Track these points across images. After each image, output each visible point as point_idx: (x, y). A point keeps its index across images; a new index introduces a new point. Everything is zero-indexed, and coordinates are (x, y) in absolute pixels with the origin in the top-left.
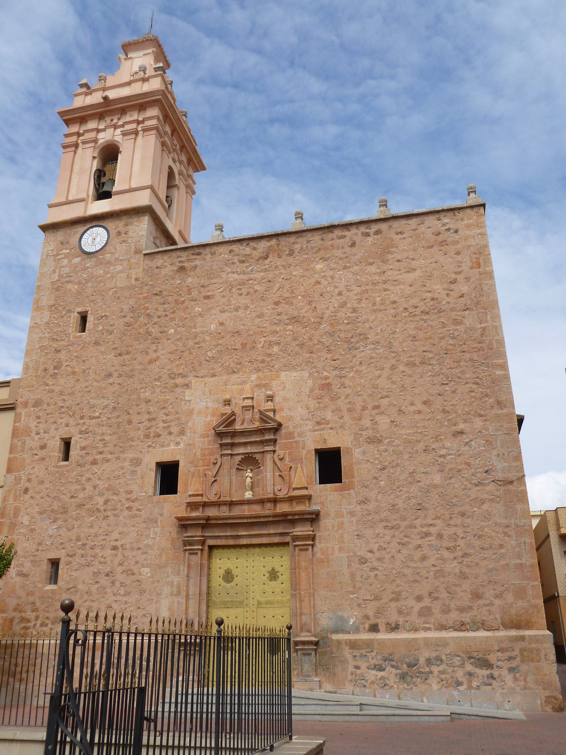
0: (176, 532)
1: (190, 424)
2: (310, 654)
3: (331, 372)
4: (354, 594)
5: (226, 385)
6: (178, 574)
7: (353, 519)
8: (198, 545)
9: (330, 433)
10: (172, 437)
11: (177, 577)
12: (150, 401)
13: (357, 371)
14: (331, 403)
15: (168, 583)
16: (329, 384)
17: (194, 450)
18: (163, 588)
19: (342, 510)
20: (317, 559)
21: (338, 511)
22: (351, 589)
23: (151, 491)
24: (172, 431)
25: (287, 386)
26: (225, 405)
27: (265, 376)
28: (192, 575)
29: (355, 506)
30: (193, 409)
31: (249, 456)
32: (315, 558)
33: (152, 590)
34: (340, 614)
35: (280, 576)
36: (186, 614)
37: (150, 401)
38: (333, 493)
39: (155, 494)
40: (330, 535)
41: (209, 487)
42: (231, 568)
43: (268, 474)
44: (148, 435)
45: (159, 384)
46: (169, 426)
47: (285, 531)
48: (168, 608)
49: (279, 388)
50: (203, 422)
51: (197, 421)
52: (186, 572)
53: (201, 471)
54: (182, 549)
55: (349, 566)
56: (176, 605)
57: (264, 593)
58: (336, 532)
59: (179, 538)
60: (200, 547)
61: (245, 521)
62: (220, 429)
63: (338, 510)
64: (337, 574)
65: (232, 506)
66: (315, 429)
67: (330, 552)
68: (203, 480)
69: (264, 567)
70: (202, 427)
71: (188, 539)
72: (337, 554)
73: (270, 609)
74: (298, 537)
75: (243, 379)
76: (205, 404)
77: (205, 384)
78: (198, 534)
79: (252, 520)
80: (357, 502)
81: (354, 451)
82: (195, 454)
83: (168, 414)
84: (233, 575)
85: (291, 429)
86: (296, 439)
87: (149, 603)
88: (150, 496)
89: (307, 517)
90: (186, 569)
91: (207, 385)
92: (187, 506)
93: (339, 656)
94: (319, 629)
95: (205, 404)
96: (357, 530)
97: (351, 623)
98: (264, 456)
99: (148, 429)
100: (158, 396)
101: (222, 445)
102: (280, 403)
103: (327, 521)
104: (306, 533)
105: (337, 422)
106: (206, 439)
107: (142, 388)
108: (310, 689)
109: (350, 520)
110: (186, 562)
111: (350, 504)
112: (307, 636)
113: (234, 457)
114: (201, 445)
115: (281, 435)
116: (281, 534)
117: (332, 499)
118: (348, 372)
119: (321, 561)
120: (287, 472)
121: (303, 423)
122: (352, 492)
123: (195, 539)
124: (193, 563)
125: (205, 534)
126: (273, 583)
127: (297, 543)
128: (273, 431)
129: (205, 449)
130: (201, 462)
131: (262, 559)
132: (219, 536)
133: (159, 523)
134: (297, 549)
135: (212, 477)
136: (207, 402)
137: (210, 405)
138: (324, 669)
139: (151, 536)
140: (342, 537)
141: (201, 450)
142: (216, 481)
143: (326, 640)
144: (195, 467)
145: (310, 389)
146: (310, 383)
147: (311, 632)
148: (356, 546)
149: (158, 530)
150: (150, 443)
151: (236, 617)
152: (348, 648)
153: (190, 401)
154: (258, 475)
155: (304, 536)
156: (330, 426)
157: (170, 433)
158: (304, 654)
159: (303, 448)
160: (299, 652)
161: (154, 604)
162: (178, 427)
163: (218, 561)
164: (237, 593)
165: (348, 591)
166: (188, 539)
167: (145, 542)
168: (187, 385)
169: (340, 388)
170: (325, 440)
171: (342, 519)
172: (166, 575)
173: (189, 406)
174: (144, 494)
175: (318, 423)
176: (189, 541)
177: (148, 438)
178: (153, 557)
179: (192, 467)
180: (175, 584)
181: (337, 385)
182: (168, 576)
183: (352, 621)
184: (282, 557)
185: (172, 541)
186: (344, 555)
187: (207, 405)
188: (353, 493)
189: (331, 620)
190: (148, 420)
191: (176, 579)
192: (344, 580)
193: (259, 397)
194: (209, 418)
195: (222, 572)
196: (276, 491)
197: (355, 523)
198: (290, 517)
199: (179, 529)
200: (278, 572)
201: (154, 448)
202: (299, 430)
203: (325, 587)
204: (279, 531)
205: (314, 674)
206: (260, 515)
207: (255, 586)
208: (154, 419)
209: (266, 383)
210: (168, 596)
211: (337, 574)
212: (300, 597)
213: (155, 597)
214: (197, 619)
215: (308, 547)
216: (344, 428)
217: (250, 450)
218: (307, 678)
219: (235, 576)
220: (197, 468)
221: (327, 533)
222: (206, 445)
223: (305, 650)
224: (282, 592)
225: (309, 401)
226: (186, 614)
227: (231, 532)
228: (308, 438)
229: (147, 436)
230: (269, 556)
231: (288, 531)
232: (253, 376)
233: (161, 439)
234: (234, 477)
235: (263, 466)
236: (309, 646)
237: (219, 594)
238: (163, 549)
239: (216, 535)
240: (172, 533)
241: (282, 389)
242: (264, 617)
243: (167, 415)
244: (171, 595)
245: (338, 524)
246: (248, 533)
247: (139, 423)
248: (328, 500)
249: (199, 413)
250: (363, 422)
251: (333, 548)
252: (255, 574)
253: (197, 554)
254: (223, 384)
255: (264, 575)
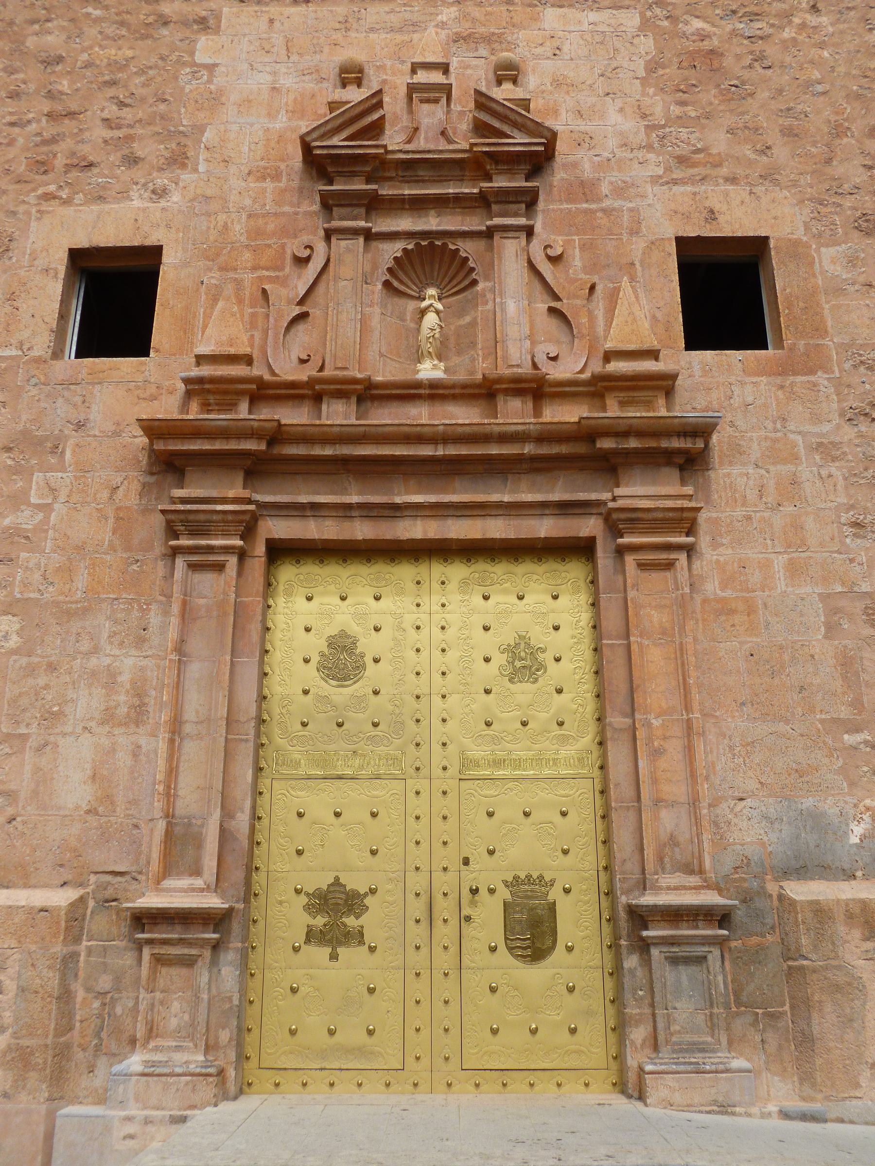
0: (136, 486)
1: (209, 135)
2: (701, 960)
3: (717, 21)
4: (857, 730)
5: (347, 30)
6: (140, 642)
7: (833, 470)
8: (226, 534)
9: (726, 194)
10: (138, 173)
11: (133, 652)
12: (60, 59)
13: (803, 26)
14: (721, 108)
15: (94, 674)
16: (712, 52)
17: (222, 217)
18: (71, 694)
19: (792, 436)
20: (705, 601)
21: (775, 441)
22: (844, 712)
23: (42, 344)
24: (140, 154)
25: (566, 48)
26: (344, 86)
27: (488, 14)
28: (196, 644)
29: (838, 427)
30: (221, 92)
31: (431, 244)
32: (698, 599)
33: (24, 701)
34: (808, 803)
35: (552, 666)
36: (170, 794)
37: (60, 59)
38: (755, 379)
39: (57, 354)
40: (749, 518)
41: (276, 335)
42: (354, 629)
43: (512, 307)
44: (43, 163)
45: (98, 13)
46: (129, 138)
47: (582, 496)
48: (89, 772)
49: (540, 50)
50: (260, 133)
51: (235, 127)
52: (173, 634)
53: (247, 283)
54: (159, 549)
55: (831, 629)
56: (123, 759)
57: (488, 724)
58: (772, 509)
59: (145, 511)
60: (239, 543)
61: (426, 451)
62: (335, 141)
63: (773, 435)
64: (786, 657)
65: (369, 404)
66: (675, 176)
67: (755, 577)
68: (253, 315)
69: (486, 629)
70: (253, 147)
71: (188, 507)
72: (781, 585)
73: (511, 785)
74: (639, 515)
75: (407, 16)
76: (269, 78)
77: (271, 21)
78: (231, 494)
79: (452, 450)
80: (842, 414)
81: (818, 250)
82: (225, 226)
83: (128, 101)
84: (362, 655)
85: (587, 171)
86: (606, 203)
87: (7, 750)
88: (38, 360)
89: (676, 443)
90: (174, 621)
91: (277, 24)
92: (189, 394)
93: (826, 968)
94: (729, 862)
95: (269, 78)
96: (852, 507)
97: (854, 840)
98: (491, 248)
99: (45, 142)
100: (91, 47)
101: (328, 203)
102: (543, 92)
103: (736, 470)
104: (670, 504)
105: (750, 163)
106: (269, 185)
107: (33, 22)
108: (715, 1102)
109: (824, 473)
110: (177, 596)
111: (816, 418)
112: (685, 888)
113: (374, 244)
114: (248, 202)
115: (551, 186)
116: (565, 508)
117: (750, 399)
118: (772, 25)
119: (725, 609)
120: (579, 302)
121: (631, 156)
122: (821, 378)
123: (219, 507)
124: (202, 601)
125: (258, 497)
126: (523, 691)
127: (626, 540)
128: (526, 167)
129: (264, 216)
130: (247, 255)
131: (478, 600)
132: (314, 506)
133: (68, 455)
134: (630, 560)
135: (289, 302)
136: (274, 73)
137: (287, 81)
138: (756, 1020)
139: (34, 500)
140: (797, 527)
141: (250, 216)
142: (303, 316)
143: (759, 903)
144: (221, 269)
145: (650, 60)
146: (647, 44)
147: (701, 872)
148: (852, 561)
149: (63, 479)
150: (52, 188)
151: (374, 815)
152: (857, 934)
153: (211, 68)
154: (461, 314)
155: (660, 515)
156: (724, 171)
157: (132, 161)
158: (674, 961)
159: (634, 232)
160: (655, 952)
161: (28, 755)
162: (162, 142)
163: (300, 602)
164: (375, 725)
165: (835, 721)
166: (188, 507)
167: (7, 522)
168: (202, 22)
169: (750, 66)
170: (712, 212)
171: (792, 468)
172: (85, 645)
173: (210, 81)
174: (14, 352)
175: (682, 160)
176: (191, 517)
177: (45, 172)
178: (37, 576)
179: (210, 270)
180: (125, 678)
181: (738, 57)
182: (96, 650)
183: (857, 832)
184: (555, 597)
185: (118, 519)
186: (809, 589)
187: (274, 82)
188: (826, 383)
189: (776, 825)
190: (49, 115)
191: (129, 662)
192: (817, 681)
193: (469, 71)
194: (281, 122)
195: (316, 644)
196: (541, 359)
197: (841, 483)
198: (606, 444)
199: (151, 479)
200: (544, 651)
201: (67, 202)
202: (616, 176)
203: (743, 704)
204: (556, 496)
205: (724, 1040)
206: (488, 429)
207: (451, 700)
208: (71, 115)
209: (493, 34)
210: (93, 724)
211: (786, 657)
212: (650, 740)
213: (34, 729)
214: (217, 815)
215: (673, 556)
216: (776, 182)
217: (438, 225)
218: (697, 1058)
219: (368, 660)
220: (231, 275)
221: (739, 513)
222: (268, 201)
223: (679, 944)
224: (561, 724)
225: (644, 94)
226: (170, 794)
227: (360, 493)
228: (650, 202)
229: (43, 166)
230: (506, 592)
231: (593, 496)
232: (446, 11)
233: (95, 178)
234: (377, 310)
235: (487, 278)
236: (697, 927)
237: (304, 725)
238: (80, 548)
239: (303, 499)
240: (120, 492)
241: (550, 54)
242: (490, 815)
243: (122, 104)
244: (102, 723)
245: (777, 484)
246: (432, 498)
247: (12, 124)
248: (736, 401)
249: (246, 103)
250: (838, 169)
251: (765, 566)
252: (449, 653)
253: (219, 567)
254: (338, 26)
255: (487, 660)
